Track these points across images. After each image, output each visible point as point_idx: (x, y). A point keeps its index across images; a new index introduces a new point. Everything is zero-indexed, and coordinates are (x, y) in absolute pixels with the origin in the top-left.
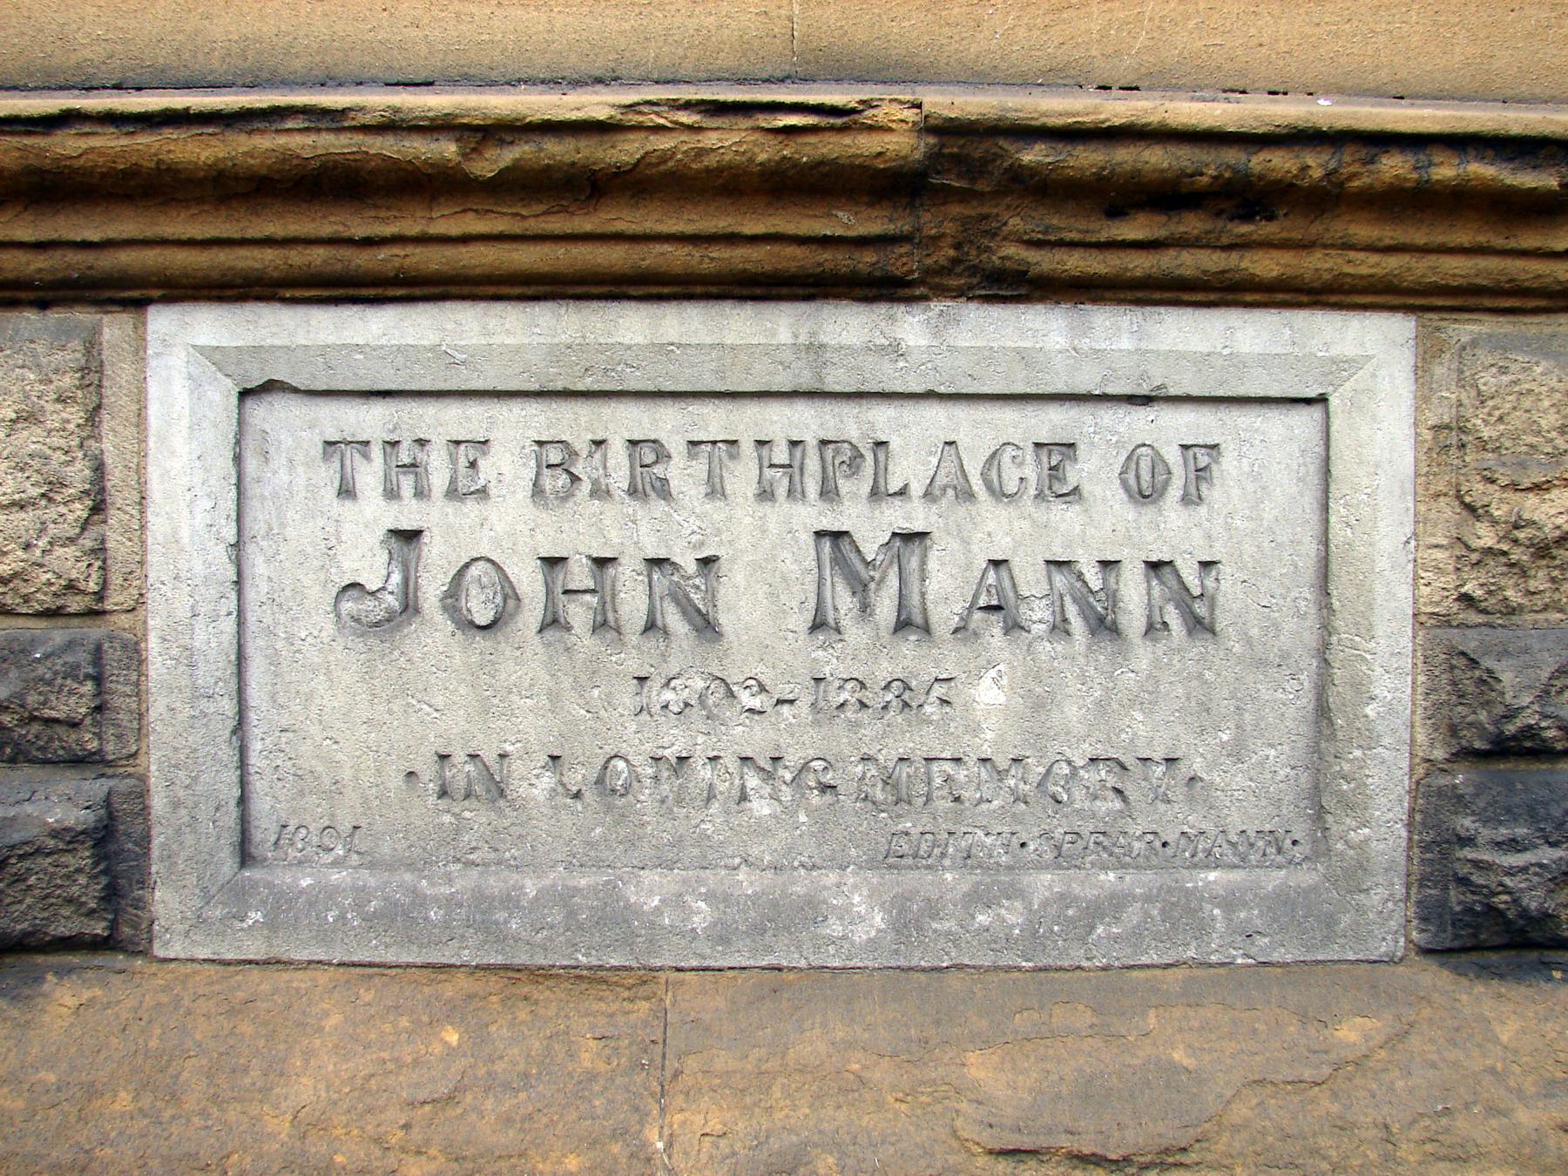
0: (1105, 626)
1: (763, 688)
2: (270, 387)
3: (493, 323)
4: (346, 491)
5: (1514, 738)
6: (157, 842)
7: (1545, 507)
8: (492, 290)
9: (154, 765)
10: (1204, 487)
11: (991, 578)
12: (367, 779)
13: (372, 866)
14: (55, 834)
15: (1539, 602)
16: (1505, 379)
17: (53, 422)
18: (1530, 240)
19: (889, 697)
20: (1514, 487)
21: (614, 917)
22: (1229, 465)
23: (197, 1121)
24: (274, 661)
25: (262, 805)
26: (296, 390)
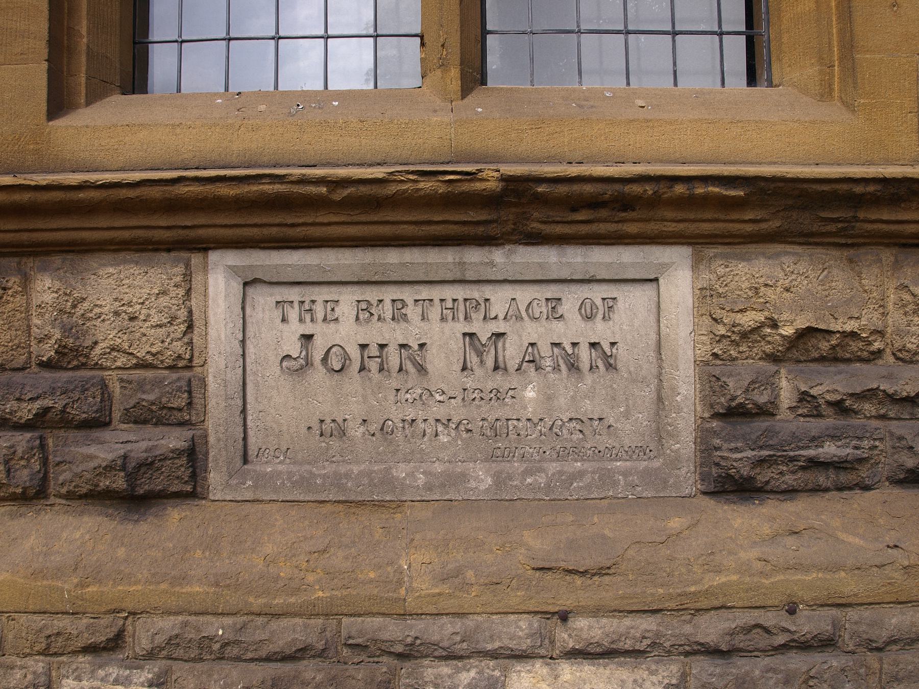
0: (573, 367)
1: (443, 393)
2: (256, 281)
3: (340, 256)
4: (284, 320)
5: (735, 408)
6: (212, 454)
7: (744, 318)
8: (339, 243)
9: (210, 425)
10: (611, 314)
11: (530, 349)
12: (292, 430)
13: (294, 463)
14: (173, 451)
15: (744, 356)
16: (728, 270)
17: (173, 294)
18: (735, 216)
19: (492, 395)
20: (732, 311)
21: (388, 481)
22: (620, 304)
23: (227, 561)
24: (257, 385)
25: (252, 440)
26: (265, 282)
